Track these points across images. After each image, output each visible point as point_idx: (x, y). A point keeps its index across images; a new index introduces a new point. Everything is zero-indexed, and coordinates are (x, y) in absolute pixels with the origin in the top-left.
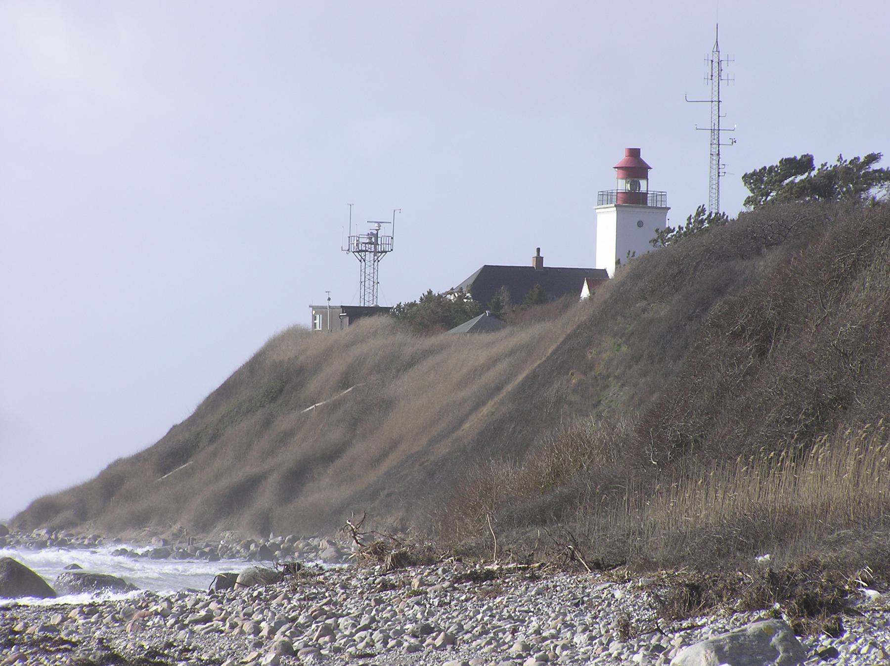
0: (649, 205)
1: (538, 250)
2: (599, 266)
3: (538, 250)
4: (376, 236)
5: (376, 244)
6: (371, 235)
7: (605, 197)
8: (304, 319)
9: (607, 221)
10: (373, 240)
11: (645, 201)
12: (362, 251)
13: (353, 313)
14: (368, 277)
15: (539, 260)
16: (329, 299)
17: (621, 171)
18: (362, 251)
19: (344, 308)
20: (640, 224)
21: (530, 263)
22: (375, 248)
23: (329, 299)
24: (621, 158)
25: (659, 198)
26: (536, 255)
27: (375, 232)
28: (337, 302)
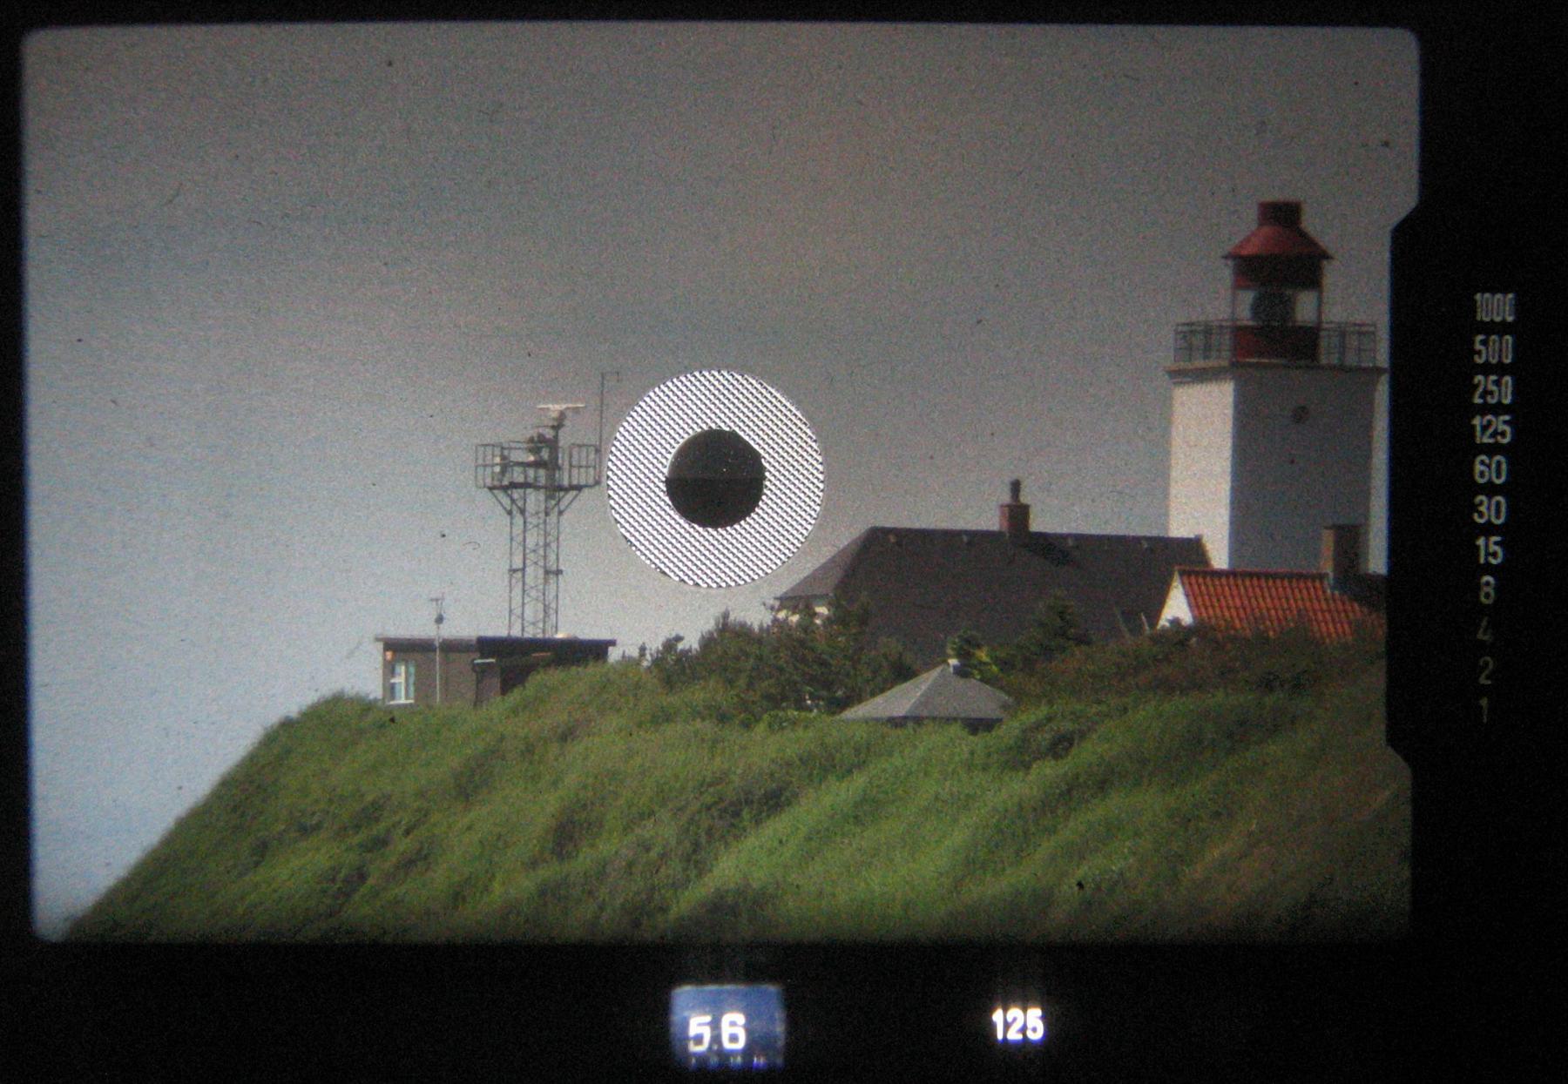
0: (1324, 361)
1: (1016, 487)
2: (1179, 529)
3: (1016, 487)
4: (553, 444)
5: (551, 465)
6: (537, 444)
7: (1198, 341)
8: (363, 676)
9: (1204, 423)
10: (545, 454)
11: (1328, 355)
12: (513, 485)
13: (510, 661)
14: (531, 556)
15: (1018, 513)
16: (440, 620)
17: (1230, 262)
18: (513, 485)
19: (486, 646)
20: (1300, 415)
21: (989, 519)
22: (551, 477)
23: (440, 620)
24: (1242, 227)
25: (1353, 342)
26: (1006, 498)
27: (549, 433)
28: (463, 627)
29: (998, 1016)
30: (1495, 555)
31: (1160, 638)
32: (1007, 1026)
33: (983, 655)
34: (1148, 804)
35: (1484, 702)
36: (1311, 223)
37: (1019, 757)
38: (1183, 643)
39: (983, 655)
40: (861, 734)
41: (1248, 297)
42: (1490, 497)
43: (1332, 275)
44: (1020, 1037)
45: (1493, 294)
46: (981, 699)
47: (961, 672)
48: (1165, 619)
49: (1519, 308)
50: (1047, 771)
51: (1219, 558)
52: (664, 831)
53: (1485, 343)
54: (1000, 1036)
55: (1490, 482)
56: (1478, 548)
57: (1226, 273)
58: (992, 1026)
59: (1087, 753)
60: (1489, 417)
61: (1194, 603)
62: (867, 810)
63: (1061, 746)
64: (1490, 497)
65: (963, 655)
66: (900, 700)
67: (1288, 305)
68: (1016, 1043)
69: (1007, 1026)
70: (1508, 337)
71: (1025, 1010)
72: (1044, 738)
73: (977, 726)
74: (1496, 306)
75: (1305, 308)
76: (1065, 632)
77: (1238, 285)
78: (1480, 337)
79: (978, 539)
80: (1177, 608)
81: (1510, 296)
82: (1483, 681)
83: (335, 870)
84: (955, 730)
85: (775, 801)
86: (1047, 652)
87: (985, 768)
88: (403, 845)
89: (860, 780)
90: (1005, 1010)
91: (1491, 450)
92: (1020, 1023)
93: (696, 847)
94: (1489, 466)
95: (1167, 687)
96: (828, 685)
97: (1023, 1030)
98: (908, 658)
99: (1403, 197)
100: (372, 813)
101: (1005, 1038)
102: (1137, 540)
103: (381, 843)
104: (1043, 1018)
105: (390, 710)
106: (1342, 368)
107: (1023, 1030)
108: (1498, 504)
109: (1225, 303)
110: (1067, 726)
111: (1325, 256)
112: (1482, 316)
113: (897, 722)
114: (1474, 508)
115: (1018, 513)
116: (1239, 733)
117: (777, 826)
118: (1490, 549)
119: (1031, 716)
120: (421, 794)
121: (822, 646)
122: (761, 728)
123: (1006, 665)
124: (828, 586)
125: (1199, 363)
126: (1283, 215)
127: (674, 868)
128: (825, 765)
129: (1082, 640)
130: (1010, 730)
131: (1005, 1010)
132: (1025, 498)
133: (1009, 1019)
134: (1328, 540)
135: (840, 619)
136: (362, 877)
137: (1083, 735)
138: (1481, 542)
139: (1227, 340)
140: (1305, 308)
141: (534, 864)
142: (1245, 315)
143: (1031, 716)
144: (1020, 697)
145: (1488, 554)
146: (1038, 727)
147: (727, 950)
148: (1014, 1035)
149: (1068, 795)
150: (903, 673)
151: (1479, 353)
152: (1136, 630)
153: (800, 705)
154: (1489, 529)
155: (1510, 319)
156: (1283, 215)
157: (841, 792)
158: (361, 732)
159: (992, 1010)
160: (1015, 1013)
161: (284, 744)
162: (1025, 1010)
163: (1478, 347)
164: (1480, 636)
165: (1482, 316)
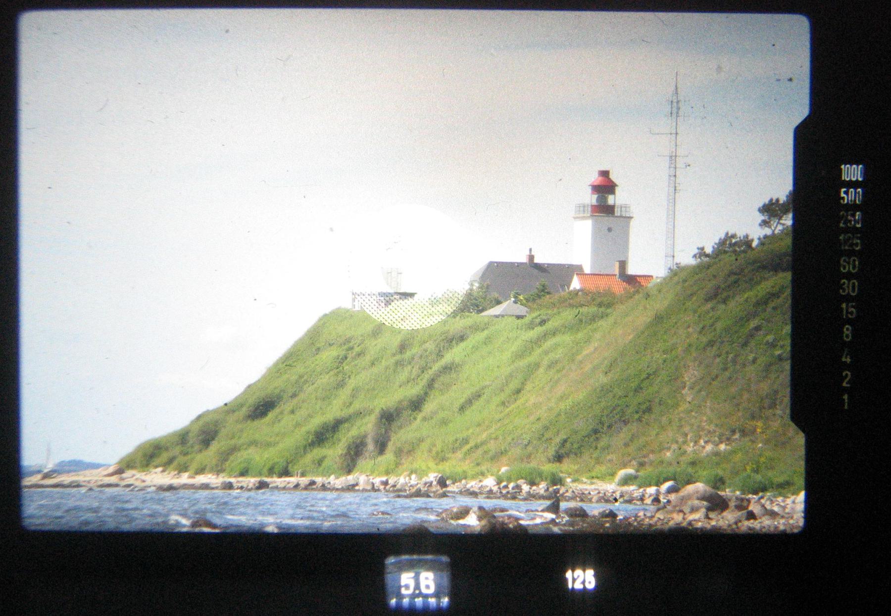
1: (531, 250)
3: (531, 250)
7: (582, 209)
11: (617, 212)
15: (531, 258)
20: (610, 230)
21: (524, 259)
24: (594, 178)
26: (528, 253)
29: (569, 575)
30: (852, 313)
31: (570, 293)
32: (574, 580)
33: (521, 297)
34: (566, 338)
35: (846, 397)
36: (612, 177)
37: (531, 326)
38: (577, 294)
39: (521, 297)
40: (486, 320)
41: (595, 196)
42: (849, 281)
43: (618, 190)
44: (581, 587)
45: (851, 165)
46: (521, 310)
47: (515, 302)
48: (571, 288)
49: (865, 173)
50: (539, 330)
51: (587, 270)
52: (430, 346)
53: (846, 193)
54: (570, 586)
55: (849, 272)
56: (842, 309)
57: (589, 190)
58: (566, 580)
59: (549, 325)
60: (850, 235)
61: (581, 282)
62: (488, 341)
63: (543, 322)
64: (849, 281)
65: (515, 297)
66: (497, 310)
67: (606, 199)
68: (580, 590)
69: (574, 580)
70: (859, 190)
71: (584, 571)
72: (538, 320)
73: (519, 317)
74: (853, 172)
75: (611, 200)
76: (544, 291)
77: (593, 193)
78: (843, 190)
79: (520, 265)
80: (576, 284)
81: (860, 166)
82: (844, 384)
83: (339, 356)
84: (514, 318)
85: (462, 338)
86: (539, 297)
87: (521, 329)
88: (357, 349)
89: (486, 332)
90: (573, 571)
91: (851, 253)
92: (582, 579)
93: (440, 351)
94: (849, 263)
95: (571, 306)
96: (477, 306)
97: (583, 583)
98: (500, 299)
99: (801, 110)
100: (348, 340)
101: (573, 588)
102: (564, 265)
103: (351, 348)
104: (595, 576)
105: (354, 312)
106: (621, 217)
107: (583, 583)
108: (854, 283)
109: (592, 199)
110: (545, 317)
111: (616, 185)
112: (845, 177)
113: (497, 316)
114: (841, 287)
115: (531, 258)
116: (594, 319)
117: (463, 345)
118: (849, 310)
119: (534, 315)
120: (362, 336)
121: (475, 294)
122: (458, 318)
123: (527, 300)
124: (477, 279)
125: (582, 215)
126: (605, 174)
127: (434, 356)
128: (476, 328)
129: (548, 293)
130: (527, 320)
131: (573, 571)
132: (533, 253)
133: (575, 577)
134: (617, 264)
135: (481, 288)
136: (346, 358)
137: (549, 320)
138: (844, 306)
139: (590, 209)
140: (611, 200)
141: (394, 355)
142: (594, 202)
143: (534, 315)
144: (532, 310)
145: (847, 312)
146: (536, 318)
147: (417, 542)
148: (578, 586)
149: (545, 336)
150: (499, 303)
151: (843, 198)
152: (564, 290)
153: (469, 311)
154: (848, 299)
155: (860, 179)
156: (605, 174)
157: (481, 336)
158: (346, 318)
159: (565, 572)
160: (579, 572)
161: (325, 320)
162: (584, 571)
163: (843, 195)
164: (844, 359)
165: (845, 177)
